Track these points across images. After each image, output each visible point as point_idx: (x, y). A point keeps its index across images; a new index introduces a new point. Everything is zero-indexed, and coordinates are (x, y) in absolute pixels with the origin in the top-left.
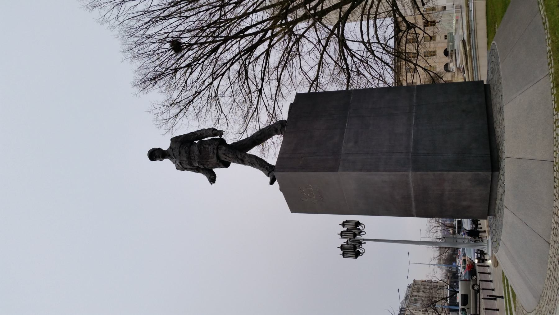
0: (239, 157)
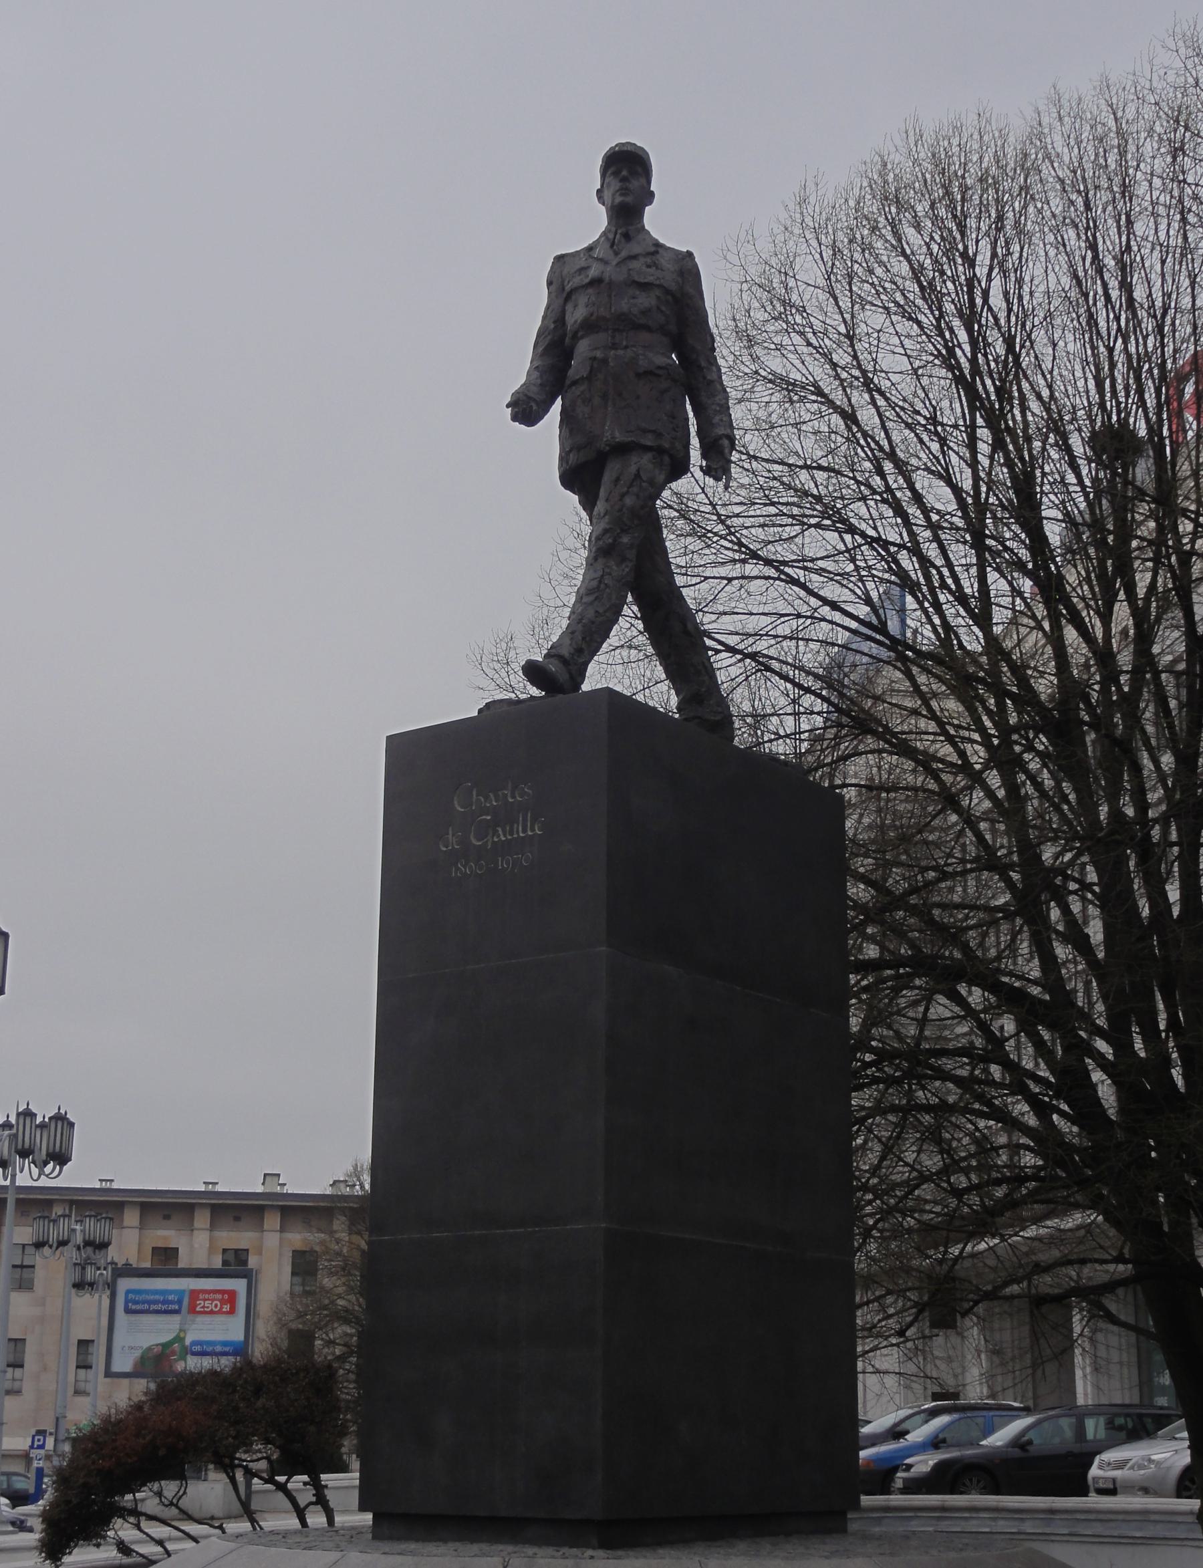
0: (625, 539)
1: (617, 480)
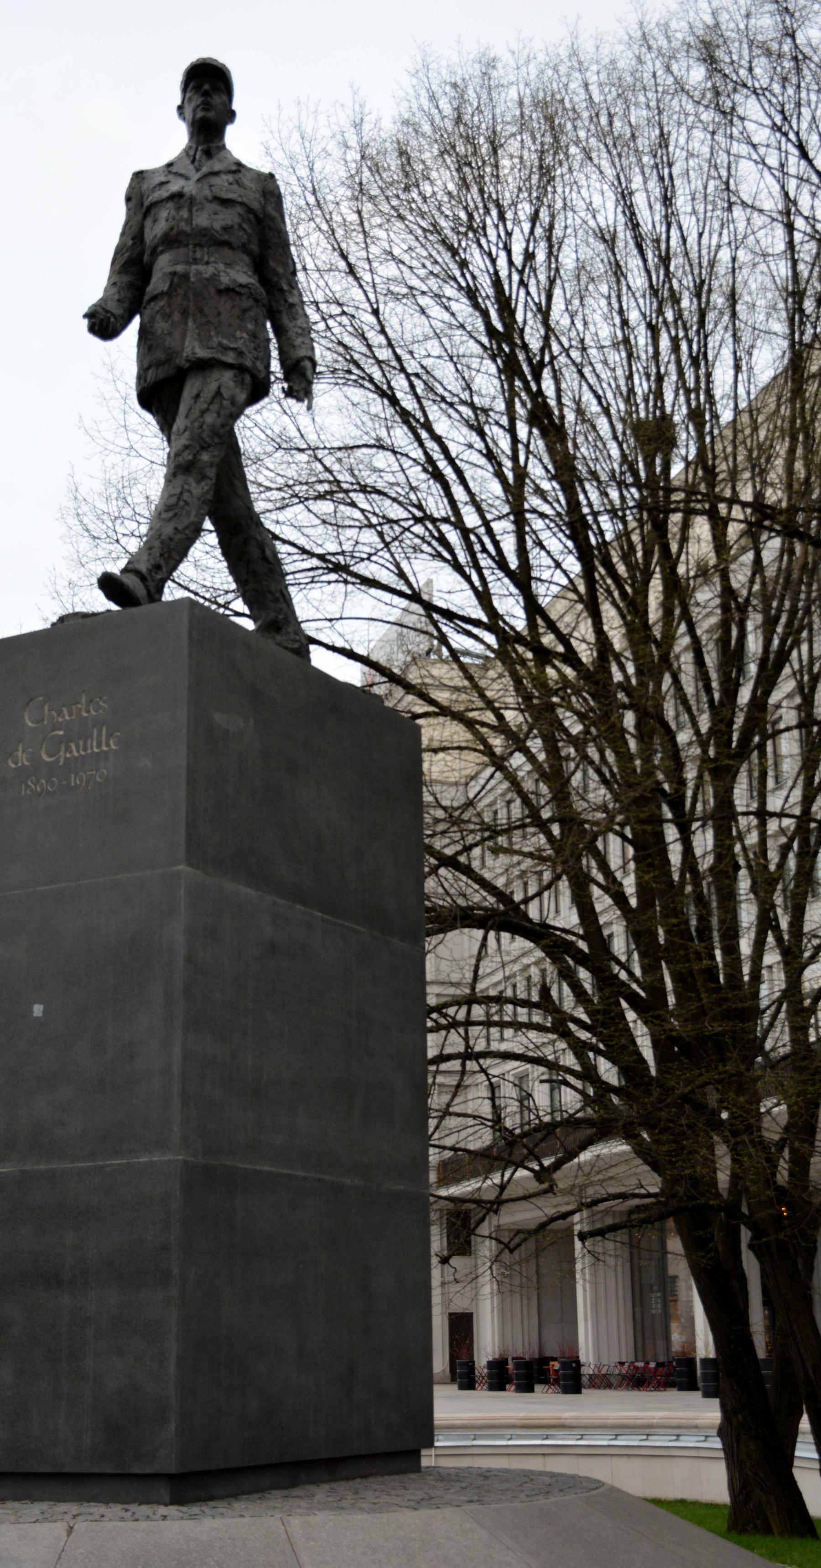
0: (205, 457)
1: (198, 396)
